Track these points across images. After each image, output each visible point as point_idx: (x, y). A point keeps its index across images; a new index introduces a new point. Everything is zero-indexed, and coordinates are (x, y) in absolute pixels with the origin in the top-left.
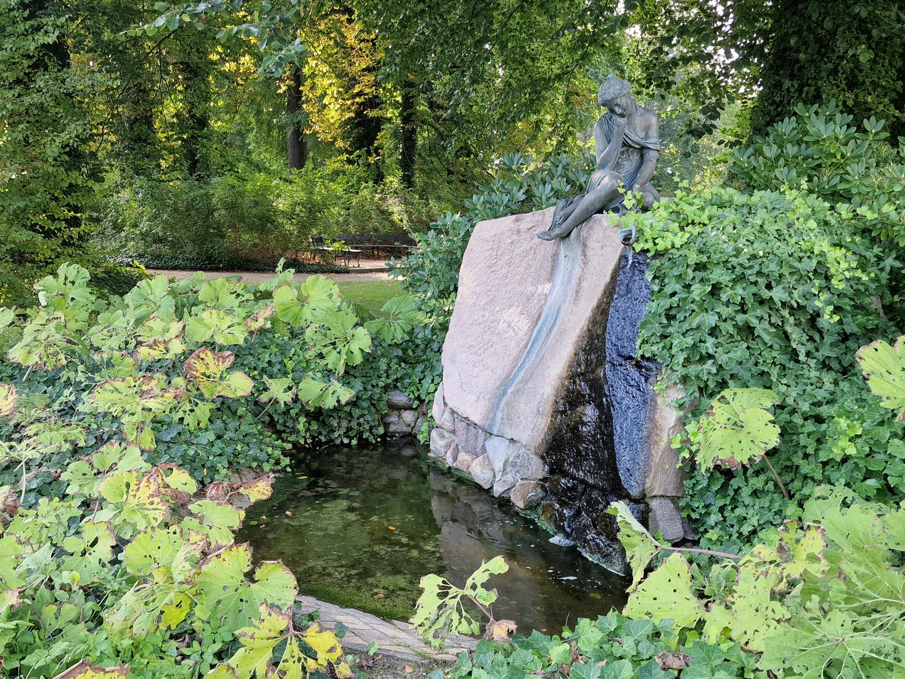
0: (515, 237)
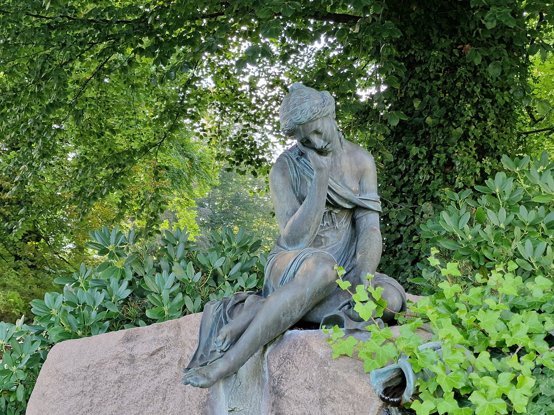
0: (125, 370)
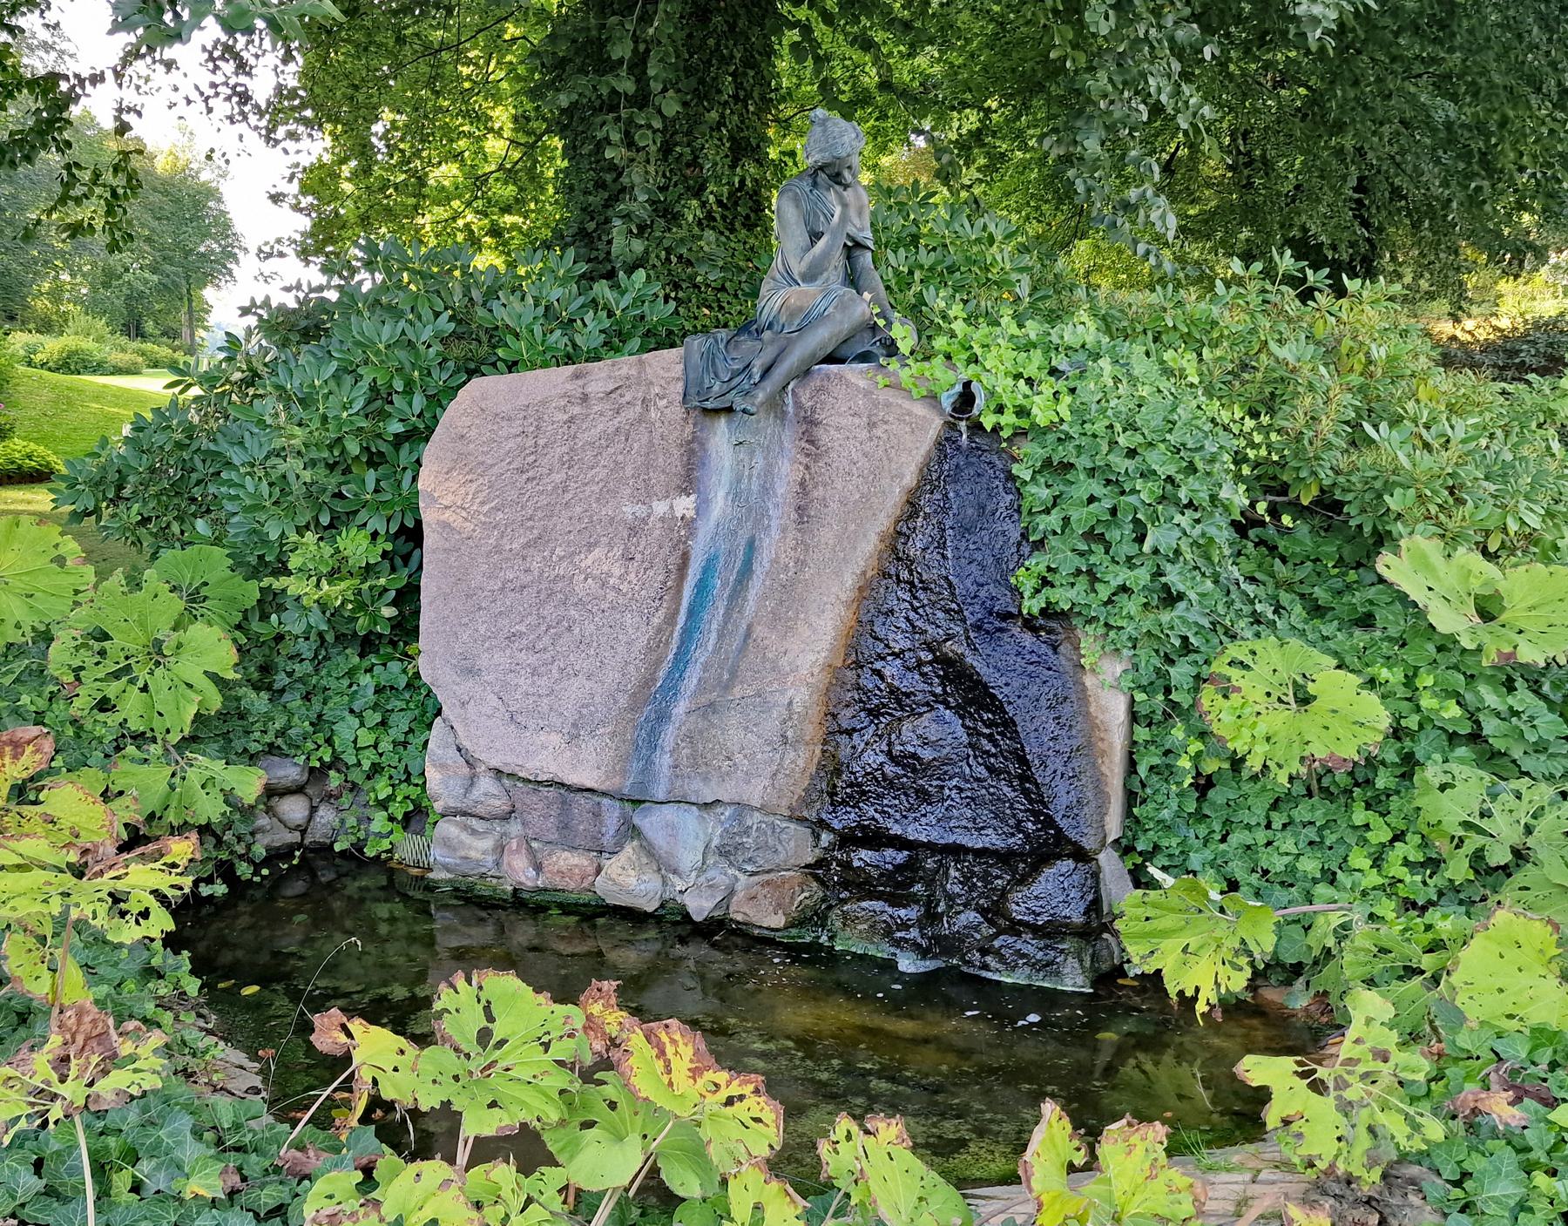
0: (576, 410)
